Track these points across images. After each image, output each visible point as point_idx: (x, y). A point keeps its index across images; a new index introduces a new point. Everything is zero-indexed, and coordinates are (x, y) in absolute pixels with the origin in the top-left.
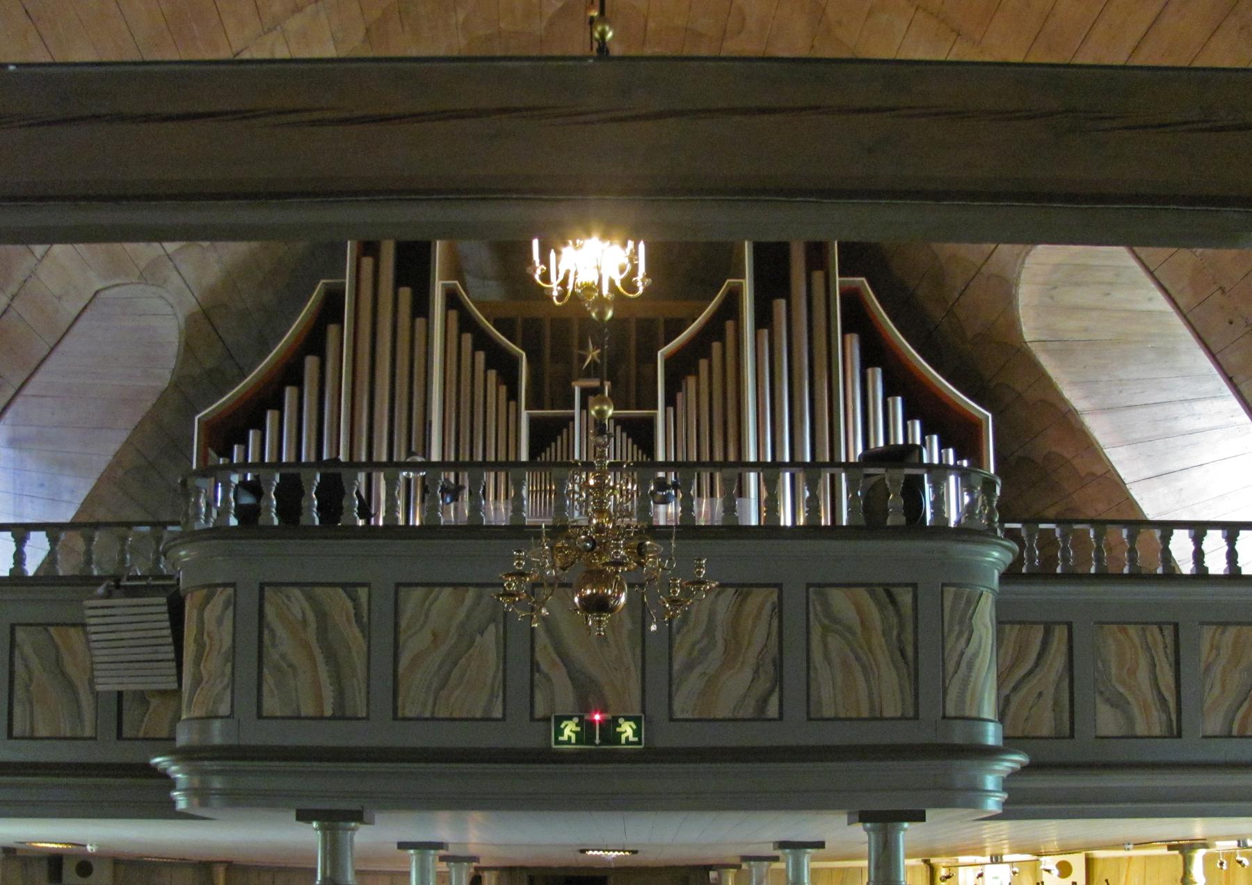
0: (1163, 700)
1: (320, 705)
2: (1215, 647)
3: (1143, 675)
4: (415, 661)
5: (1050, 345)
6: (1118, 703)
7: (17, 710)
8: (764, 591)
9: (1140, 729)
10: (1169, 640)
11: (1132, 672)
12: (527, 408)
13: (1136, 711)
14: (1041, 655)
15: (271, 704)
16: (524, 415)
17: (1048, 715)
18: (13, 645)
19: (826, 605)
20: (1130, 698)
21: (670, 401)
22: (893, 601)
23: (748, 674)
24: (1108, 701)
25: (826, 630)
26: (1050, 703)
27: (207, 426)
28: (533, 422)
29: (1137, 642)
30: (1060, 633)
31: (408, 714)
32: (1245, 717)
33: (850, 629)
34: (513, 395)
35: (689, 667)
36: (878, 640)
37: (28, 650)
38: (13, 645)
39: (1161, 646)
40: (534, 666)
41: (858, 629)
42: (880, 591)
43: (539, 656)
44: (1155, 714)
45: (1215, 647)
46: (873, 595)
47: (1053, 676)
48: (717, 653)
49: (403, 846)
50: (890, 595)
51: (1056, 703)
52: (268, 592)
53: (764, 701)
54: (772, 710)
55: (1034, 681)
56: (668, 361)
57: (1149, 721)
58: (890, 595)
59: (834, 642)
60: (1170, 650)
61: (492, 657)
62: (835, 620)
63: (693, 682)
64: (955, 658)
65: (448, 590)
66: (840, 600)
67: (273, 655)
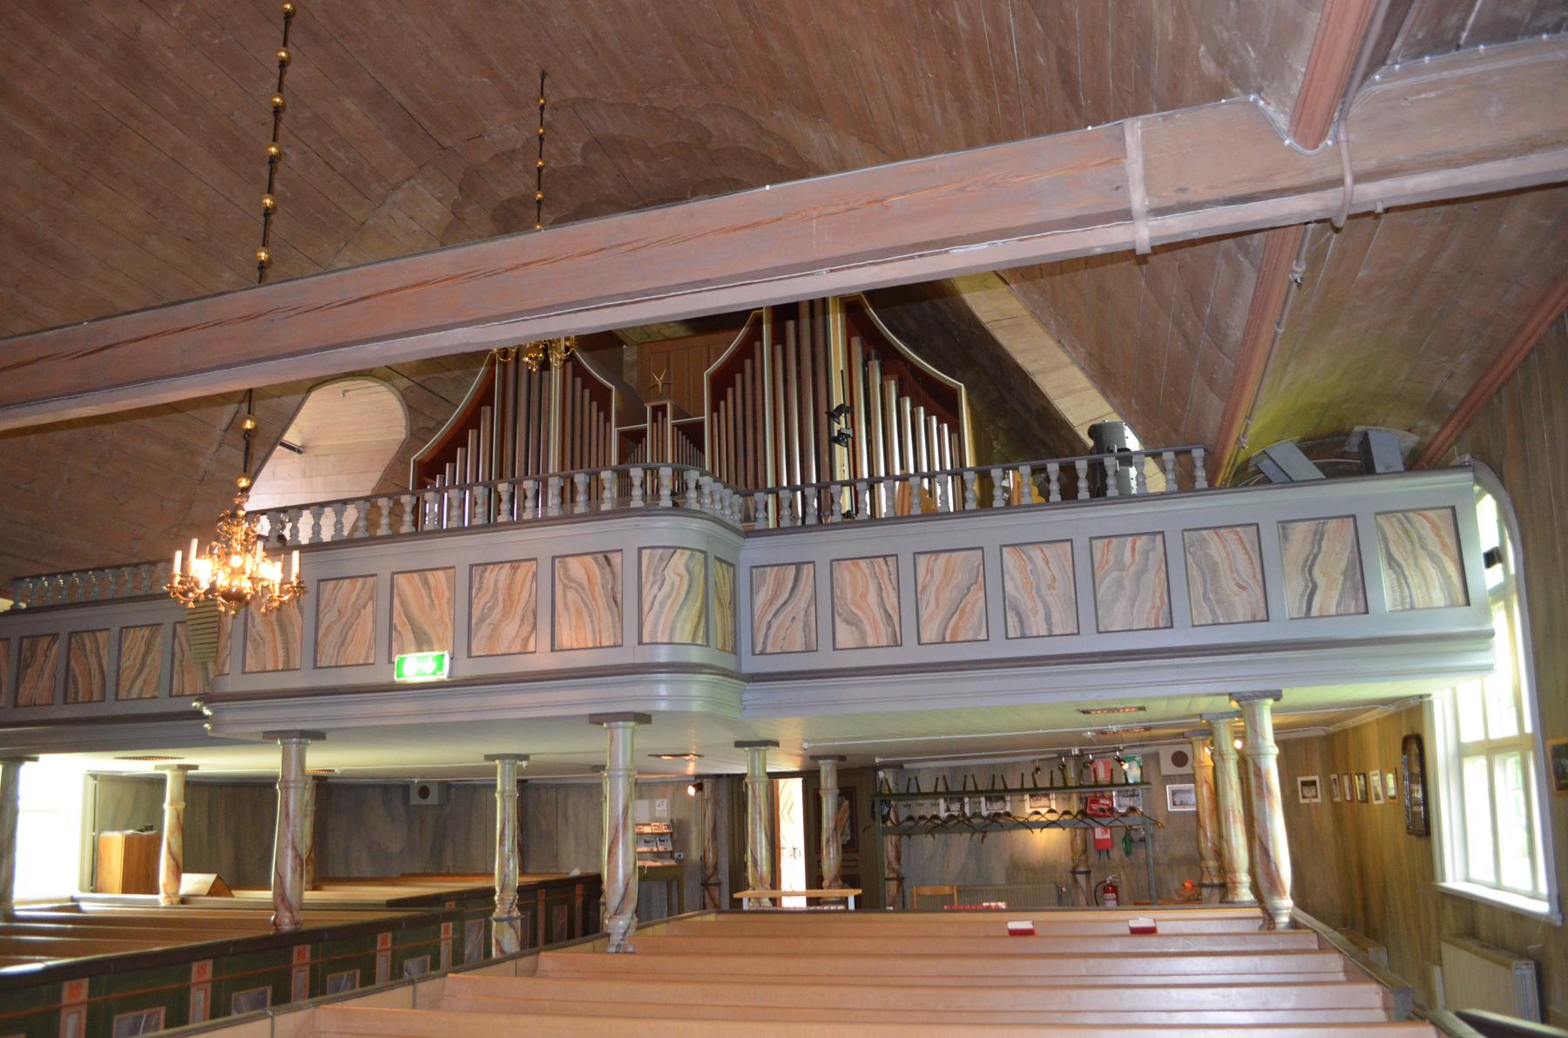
0: (889, 616)
1: (276, 662)
2: (930, 571)
3: (872, 598)
4: (329, 628)
5: (1004, 323)
6: (854, 622)
7: (175, 677)
8: (528, 564)
9: (871, 641)
10: (892, 569)
11: (864, 596)
12: (617, 425)
13: (867, 625)
14: (793, 589)
15: (251, 664)
16: (614, 432)
17: (799, 635)
18: (174, 634)
19: (566, 569)
20: (861, 615)
21: (715, 408)
22: (609, 563)
23: (517, 622)
24: (847, 621)
25: (565, 586)
26: (801, 625)
27: (418, 464)
28: (622, 434)
29: (867, 571)
30: (807, 570)
31: (324, 664)
32: (957, 624)
33: (581, 585)
34: (607, 419)
35: (482, 620)
36: (598, 590)
37: (183, 639)
38: (174, 634)
39: (886, 576)
40: (391, 627)
41: (586, 585)
42: (601, 557)
43: (395, 621)
44: (882, 628)
45: (930, 571)
46: (596, 560)
47: (803, 605)
48: (499, 609)
49: (489, 758)
50: (606, 558)
51: (805, 625)
52: (979, 553)
53: (527, 640)
54: (531, 647)
55: (789, 608)
56: (610, 390)
57: (877, 634)
58: (606, 558)
59: (571, 595)
60: (893, 577)
61: (370, 624)
62: (572, 580)
63: (483, 631)
64: (650, 598)
65: (1144, 538)
66: (573, 564)
67: (253, 632)
